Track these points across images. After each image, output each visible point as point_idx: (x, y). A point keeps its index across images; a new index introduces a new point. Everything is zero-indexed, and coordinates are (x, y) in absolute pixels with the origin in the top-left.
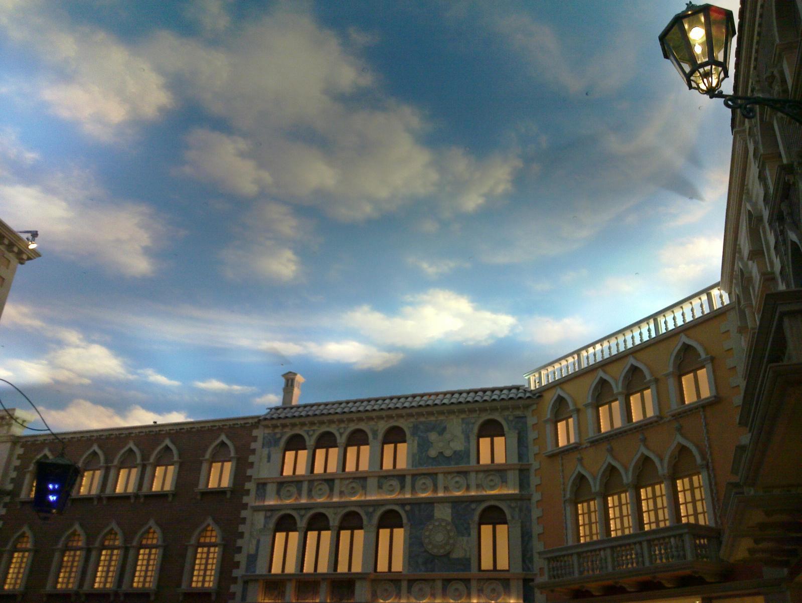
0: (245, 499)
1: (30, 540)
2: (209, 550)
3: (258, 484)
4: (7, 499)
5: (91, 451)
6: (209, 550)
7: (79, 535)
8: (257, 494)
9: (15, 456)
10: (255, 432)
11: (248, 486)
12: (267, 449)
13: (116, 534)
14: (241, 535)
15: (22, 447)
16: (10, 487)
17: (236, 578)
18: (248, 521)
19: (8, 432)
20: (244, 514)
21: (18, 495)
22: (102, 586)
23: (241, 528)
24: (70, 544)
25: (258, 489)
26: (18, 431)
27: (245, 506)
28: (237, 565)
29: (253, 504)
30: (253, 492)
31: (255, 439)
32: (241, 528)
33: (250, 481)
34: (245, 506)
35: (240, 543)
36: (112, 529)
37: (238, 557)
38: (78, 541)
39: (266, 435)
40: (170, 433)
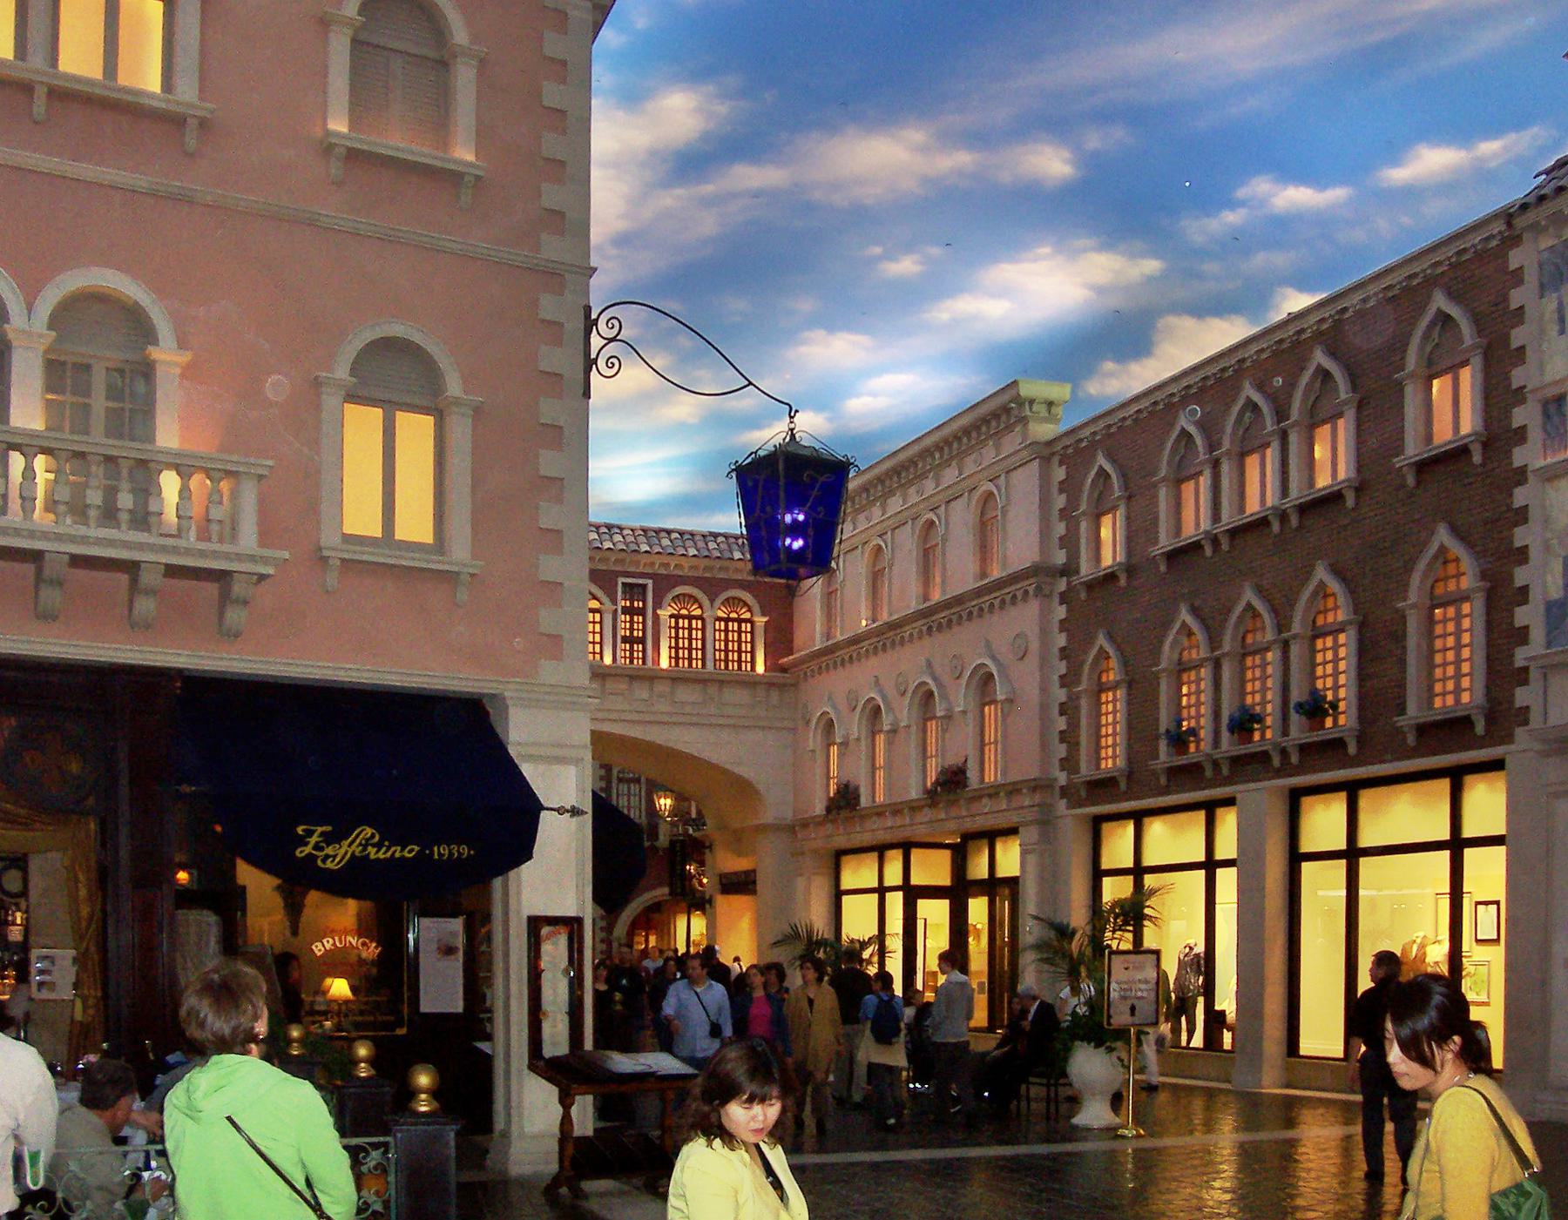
0: (1519, 456)
1: (1341, 600)
2: (1458, 611)
3: (1545, 404)
4: (1062, 585)
5: (1241, 402)
6: (1458, 611)
7: (1457, 560)
8: (1545, 430)
9: (1055, 489)
10: (1515, 259)
11: (1520, 416)
12: (1555, 295)
13: (1457, 560)
14: (1522, 555)
15: (1061, 463)
16: (1060, 558)
17: (1526, 669)
18: (1534, 513)
19: (1025, 437)
20: (1520, 496)
21: (1077, 572)
22: (1450, 700)
23: (1520, 536)
24: (1440, 589)
25: (1546, 415)
26: (1044, 431)
27: (1521, 475)
28: (1522, 635)
29: (1540, 463)
30: (1535, 435)
31: (1517, 277)
32: (1520, 536)
33: (1523, 401)
34: (1521, 475)
35: (1521, 576)
36: (1443, 550)
37: (1522, 616)
38: (1459, 575)
39: (1546, 255)
40: (1321, 333)
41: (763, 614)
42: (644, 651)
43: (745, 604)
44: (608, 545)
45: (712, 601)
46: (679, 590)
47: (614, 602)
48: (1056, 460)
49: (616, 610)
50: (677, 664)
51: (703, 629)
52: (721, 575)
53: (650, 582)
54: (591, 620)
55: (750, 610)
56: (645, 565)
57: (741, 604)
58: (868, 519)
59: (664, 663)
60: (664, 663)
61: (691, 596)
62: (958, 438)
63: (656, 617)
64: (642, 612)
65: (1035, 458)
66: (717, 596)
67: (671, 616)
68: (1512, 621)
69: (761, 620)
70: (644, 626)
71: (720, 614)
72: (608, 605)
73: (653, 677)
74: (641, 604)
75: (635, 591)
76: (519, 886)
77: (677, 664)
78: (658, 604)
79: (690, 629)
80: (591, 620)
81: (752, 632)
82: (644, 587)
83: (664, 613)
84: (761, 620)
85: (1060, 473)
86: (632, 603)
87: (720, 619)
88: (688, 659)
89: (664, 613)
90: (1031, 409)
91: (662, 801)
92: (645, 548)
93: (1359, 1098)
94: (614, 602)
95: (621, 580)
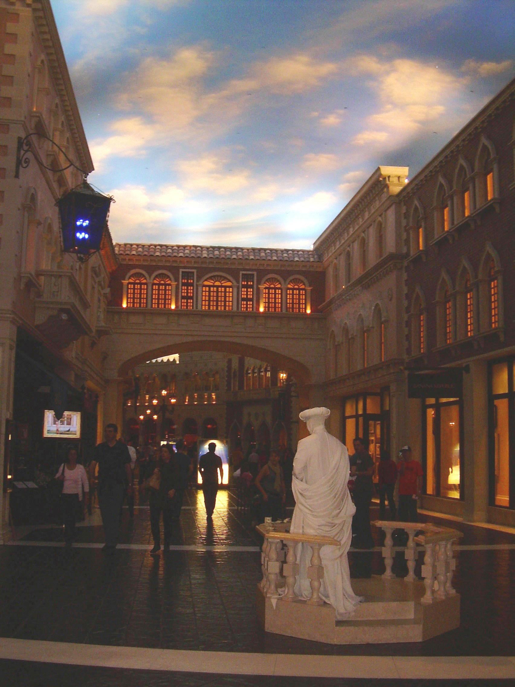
16: (405, 250)
41: (310, 286)
42: (253, 305)
43: (278, 281)
44: (234, 256)
45: (150, 276)
46: (133, 271)
47: (238, 282)
48: (402, 204)
49: (239, 286)
50: (269, 310)
51: (281, 294)
52: (211, 266)
53: (255, 273)
54: (264, 292)
55: (304, 284)
56: (317, 267)
57: (142, 276)
58: (344, 239)
59: (262, 309)
60: (262, 309)
61: (165, 275)
62: (366, 197)
63: (258, 289)
64: (251, 286)
65: (391, 206)
66: (153, 272)
67: (266, 288)
68: (308, 251)
69: (309, 289)
70: (253, 293)
71: (289, 286)
72: (235, 284)
73: (258, 315)
74: (251, 283)
75: (187, 275)
76: (73, 421)
77: (269, 310)
78: (259, 283)
79: (141, 289)
80: (189, 289)
81: (305, 295)
82: (193, 273)
83: (262, 287)
84: (309, 289)
85: (404, 209)
86: (188, 281)
87: (290, 289)
88: (292, 308)
89: (262, 287)
90: (389, 180)
91: (282, 375)
92: (252, 257)
93: (508, 499)
94: (238, 282)
95: (241, 273)
